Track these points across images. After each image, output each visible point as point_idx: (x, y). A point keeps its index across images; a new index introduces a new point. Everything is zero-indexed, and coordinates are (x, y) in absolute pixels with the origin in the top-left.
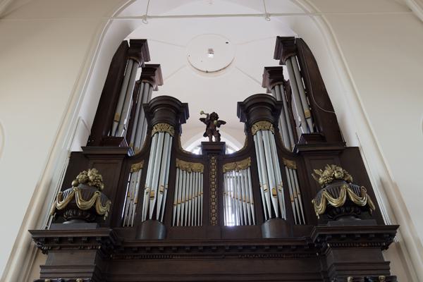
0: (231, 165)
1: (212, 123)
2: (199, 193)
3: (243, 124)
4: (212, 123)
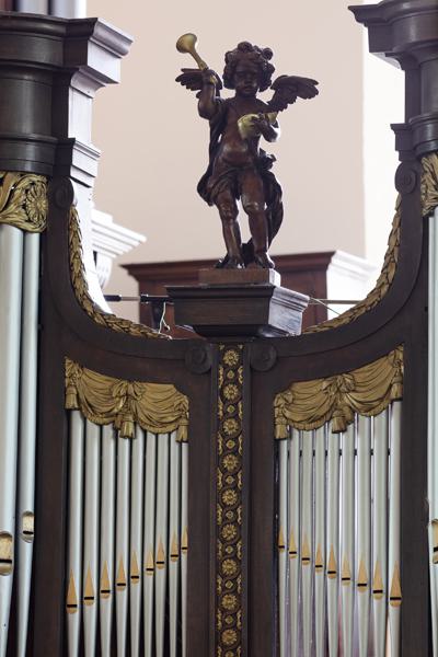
0: (311, 393)
1: (242, 99)
2: (174, 549)
3: (215, 206)
4: (242, 99)
